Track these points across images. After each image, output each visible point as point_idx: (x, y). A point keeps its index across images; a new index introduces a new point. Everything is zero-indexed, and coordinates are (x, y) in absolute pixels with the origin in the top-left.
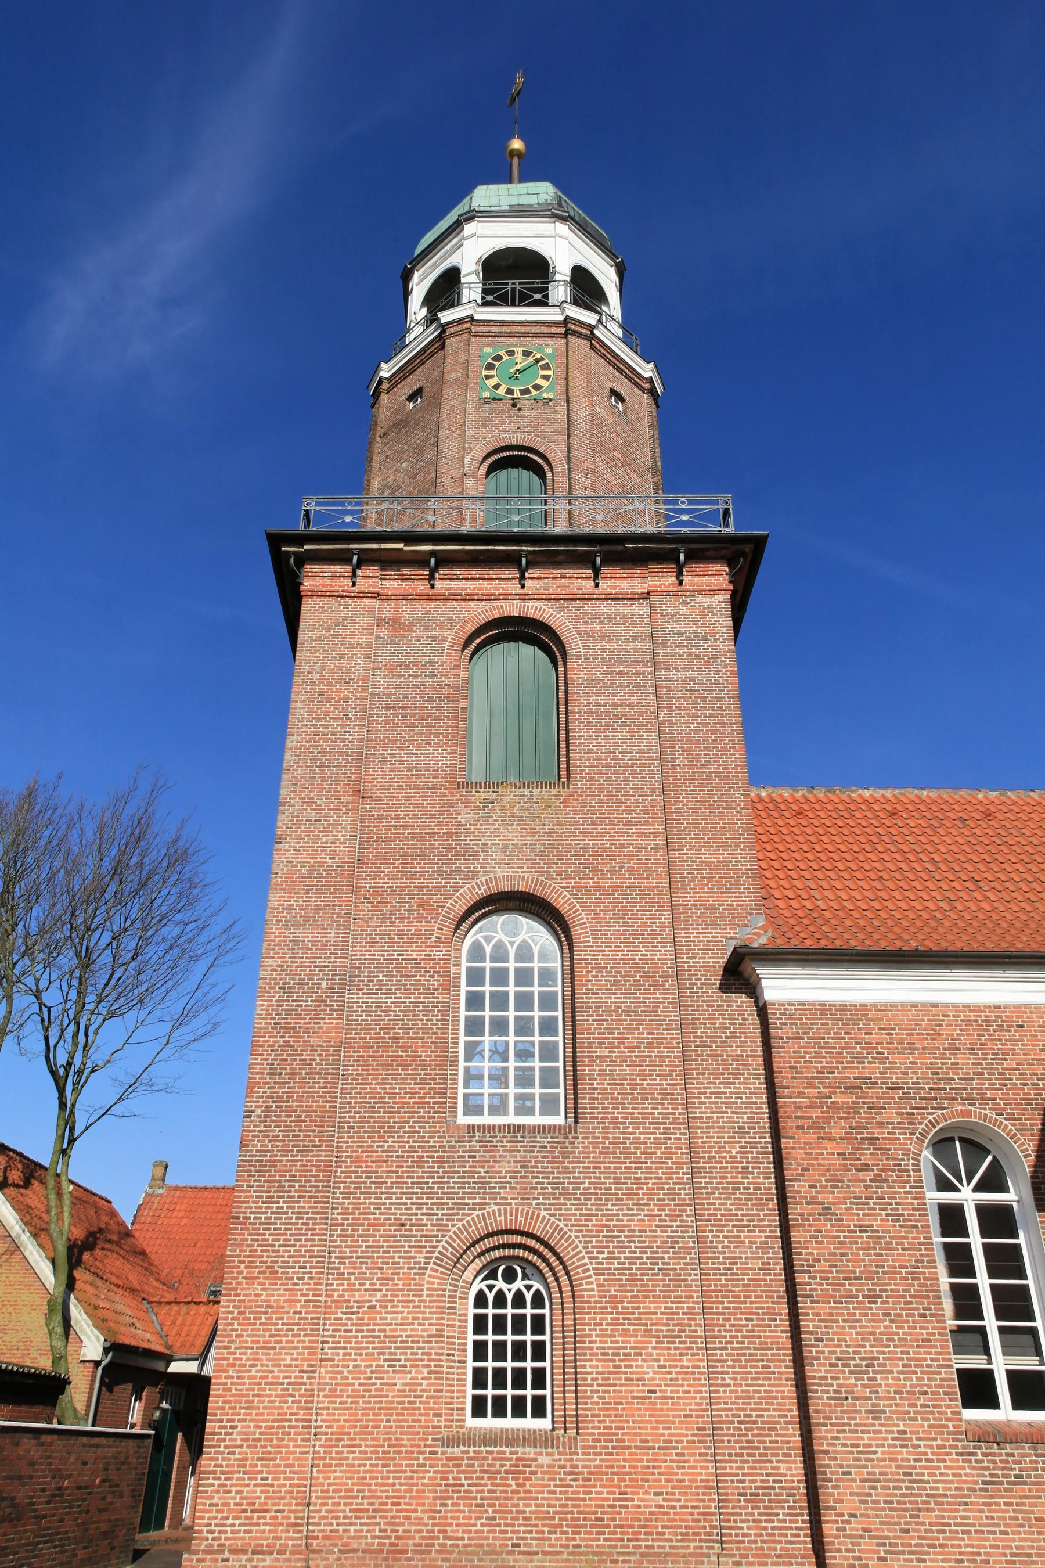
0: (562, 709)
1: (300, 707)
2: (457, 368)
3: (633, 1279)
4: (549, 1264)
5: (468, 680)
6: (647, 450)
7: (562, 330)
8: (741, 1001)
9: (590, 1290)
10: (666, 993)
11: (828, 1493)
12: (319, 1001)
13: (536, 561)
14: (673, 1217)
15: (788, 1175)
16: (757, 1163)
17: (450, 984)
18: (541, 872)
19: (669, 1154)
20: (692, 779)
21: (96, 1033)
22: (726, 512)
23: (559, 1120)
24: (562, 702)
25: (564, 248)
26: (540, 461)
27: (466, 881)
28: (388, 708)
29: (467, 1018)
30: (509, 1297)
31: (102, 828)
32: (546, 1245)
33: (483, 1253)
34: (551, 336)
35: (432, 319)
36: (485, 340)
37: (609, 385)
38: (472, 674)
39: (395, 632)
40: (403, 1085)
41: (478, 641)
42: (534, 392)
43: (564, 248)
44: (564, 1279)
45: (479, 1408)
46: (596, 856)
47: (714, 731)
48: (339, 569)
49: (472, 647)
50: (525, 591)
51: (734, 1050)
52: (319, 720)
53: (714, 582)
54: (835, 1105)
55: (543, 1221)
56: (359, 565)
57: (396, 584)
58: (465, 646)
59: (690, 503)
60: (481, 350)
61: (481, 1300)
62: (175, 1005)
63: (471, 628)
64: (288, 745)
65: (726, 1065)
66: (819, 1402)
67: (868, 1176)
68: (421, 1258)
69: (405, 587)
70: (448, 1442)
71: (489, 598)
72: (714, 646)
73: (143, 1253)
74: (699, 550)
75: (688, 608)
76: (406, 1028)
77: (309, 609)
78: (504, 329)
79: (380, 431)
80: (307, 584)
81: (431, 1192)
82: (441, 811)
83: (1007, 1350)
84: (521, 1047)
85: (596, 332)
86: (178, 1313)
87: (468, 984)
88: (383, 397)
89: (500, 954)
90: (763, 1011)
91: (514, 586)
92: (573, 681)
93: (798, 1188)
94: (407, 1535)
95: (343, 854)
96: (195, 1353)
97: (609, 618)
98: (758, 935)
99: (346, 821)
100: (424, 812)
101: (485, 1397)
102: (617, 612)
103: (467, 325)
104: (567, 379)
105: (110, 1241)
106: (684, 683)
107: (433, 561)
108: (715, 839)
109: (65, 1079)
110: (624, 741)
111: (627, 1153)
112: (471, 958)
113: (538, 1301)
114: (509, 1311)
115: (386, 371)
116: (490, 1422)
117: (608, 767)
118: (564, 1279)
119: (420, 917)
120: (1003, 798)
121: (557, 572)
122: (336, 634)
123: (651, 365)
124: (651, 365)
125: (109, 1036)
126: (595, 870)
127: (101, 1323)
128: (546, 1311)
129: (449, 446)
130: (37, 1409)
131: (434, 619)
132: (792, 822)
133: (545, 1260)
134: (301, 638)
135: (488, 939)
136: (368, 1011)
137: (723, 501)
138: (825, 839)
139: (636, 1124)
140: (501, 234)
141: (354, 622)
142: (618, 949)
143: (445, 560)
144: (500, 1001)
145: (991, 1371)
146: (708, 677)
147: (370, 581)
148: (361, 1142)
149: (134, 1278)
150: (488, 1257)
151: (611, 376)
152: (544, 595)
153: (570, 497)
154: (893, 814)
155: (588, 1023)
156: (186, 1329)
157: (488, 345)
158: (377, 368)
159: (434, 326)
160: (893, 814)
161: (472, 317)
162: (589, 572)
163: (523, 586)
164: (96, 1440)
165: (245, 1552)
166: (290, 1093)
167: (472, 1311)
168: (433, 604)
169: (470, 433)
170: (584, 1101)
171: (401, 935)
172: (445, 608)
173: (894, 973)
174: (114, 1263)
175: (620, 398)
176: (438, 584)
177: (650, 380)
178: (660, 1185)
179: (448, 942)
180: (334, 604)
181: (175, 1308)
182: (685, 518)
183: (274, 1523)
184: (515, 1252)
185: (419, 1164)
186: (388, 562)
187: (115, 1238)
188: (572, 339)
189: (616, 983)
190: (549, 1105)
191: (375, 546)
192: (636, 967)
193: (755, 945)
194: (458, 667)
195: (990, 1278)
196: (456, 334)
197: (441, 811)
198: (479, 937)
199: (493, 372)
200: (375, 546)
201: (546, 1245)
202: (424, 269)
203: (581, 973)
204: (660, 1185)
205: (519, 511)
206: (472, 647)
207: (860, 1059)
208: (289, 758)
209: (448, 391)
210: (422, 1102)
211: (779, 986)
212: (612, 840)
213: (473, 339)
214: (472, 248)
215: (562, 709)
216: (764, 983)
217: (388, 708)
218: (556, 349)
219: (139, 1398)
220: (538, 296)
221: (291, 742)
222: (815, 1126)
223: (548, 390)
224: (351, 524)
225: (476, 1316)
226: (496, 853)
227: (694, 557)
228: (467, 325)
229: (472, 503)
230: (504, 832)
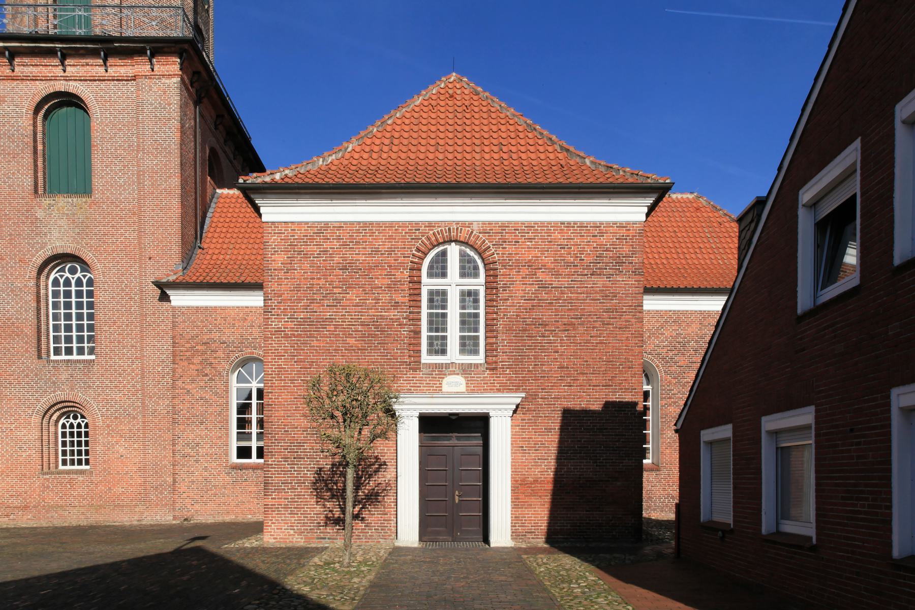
10: (135, 302)
14: (133, 395)
18: (78, 243)
19: (133, 371)
30: (75, 425)
40: (18, 343)
45: (64, 463)
46: (105, 235)
47: (166, 165)
50: (66, 74)
51: (163, 327)
55: (79, 396)
65: (158, 334)
67: (206, 378)
72: (169, 113)
75: (157, 86)
81: (32, 387)
82: (27, 211)
91: (58, 71)
106: (152, 136)
108: (162, 226)
111: (115, 371)
113: (87, 426)
116: (68, 467)
117: (112, 186)
119: (20, 267)
121: (84, 61)
126: (104, 242)
131: (17, 93)
135: (62, 276)
146: (165, 132)
162: (56, 62)
163: (65, 71)
168: (15, 83)
171: (12, 275)
172: (22, 85)
176: (17, 69)
184: (69, 409)
185: (27, 376)
192: (122, 290)
198: (57, 275)
207: (210, 331)
210: (27, 351)
212: (113, 226)
222: (188, 359)
230: (59, 222)
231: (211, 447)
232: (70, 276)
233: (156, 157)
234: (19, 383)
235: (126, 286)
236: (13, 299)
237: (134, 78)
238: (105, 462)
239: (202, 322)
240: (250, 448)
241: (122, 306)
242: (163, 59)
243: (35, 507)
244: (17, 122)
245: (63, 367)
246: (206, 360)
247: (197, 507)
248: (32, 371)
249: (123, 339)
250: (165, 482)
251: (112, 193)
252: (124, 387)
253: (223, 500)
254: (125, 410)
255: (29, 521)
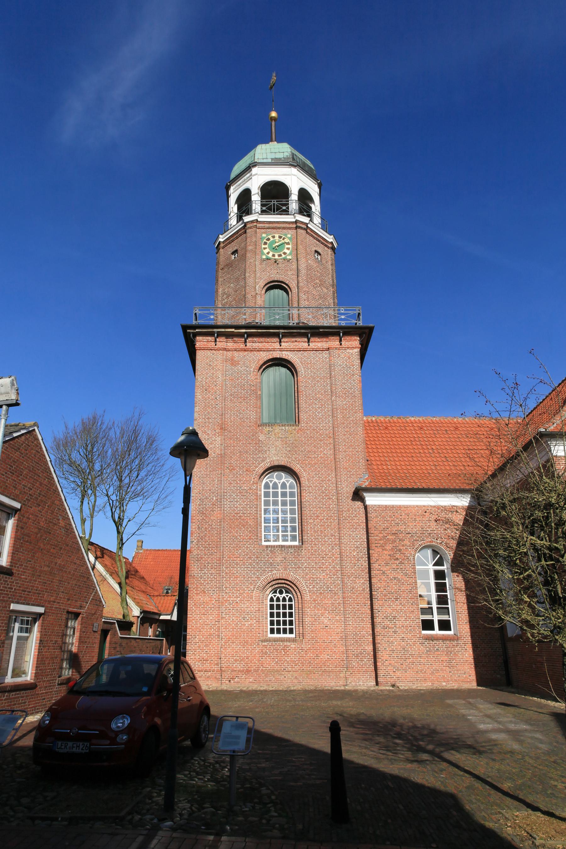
0: (296, 395)
1: (199, 395)
2: (252, 244)
3: (321, 593)
4: (294, 589)
5: (261, 383)
6: (330, 276)
7: (294, 226)
8: (359, 504)
9: (307, 597)
11: (379, 654)
12: (213, 504)
13: (285, 335)
14: (334, 575)
15: (371, 562)
16: (362, 557)
17: (258, 498)
20: (344, 423)
21: (126, 506)
22: (359, 314)
23: (296, 543)
24: (296, 392)
25: (295, 180)
26: (286, 287)
27: (263, 461)
28: (231, 395)
29: (264, 500)
30: (281, 599)
31: (122, 429)
32: (293, 583)
33: (272, 586)
34: (290, 228)
35: (240, 218)
36: (263, 230)
37: (314, 249)
38: (262, 380)
39: (232, 364)
40: (243, 532)
41: (264, 367)
42: (283, 256)
43: (295, 180)
44: (299, 594)
45: (272, 631)
47: (352, 405)
48: (210, 338)
49: (262, 369)
51: (356, 520)
52: (206, 400)
53: (354, 342)
54: (388, 539)
56: (217, 337)
57: (232, 344)
58: (259, 370)
59: (345, 310)
60: (261, 235)
61: (272, 600)
62: (155, 497)
63: (261, 362)
64: (196, 410)
65: (353, 526)
66: (378, 629)
68: (252, 587)
69: (235, 346)
70: (263, 641)
71: (268, 350)
73: (143, 578)
74: (348, 331)
75: (343, 354)
76: (244, 513)
77: (199, 355)
78: (271, 225)
79: (221, 267)
80: (198, 345)
81: (254, 567)
82: (253, 435)
83: (439, 614)
84: (283, 519)
85: (309, 225)
86: (161, 599)
87: (264, 497)
88: (221, 250)
89: (275, 486)
90: (366, 507)
91: (277, 345)
92: (300, 384)
93: (375, 566)
94: (251, 667)
95: (218, 451)
96: (169, 613)
97: (314, 359)
98: (365, 482)
99: (218, 439)
100: (247, 436)
101: (273, 605)
102: (317, 356)
103: (255, 224)
104: (297, 249)
105: (132, 575)
106: (342, 386)
107: (246, 335)
108: (351, 446)
109: (118, 524)
110: (319, 408)
111: (319, 554)
112: (265, 488)
113: (290, 600)
114: (281, 603)
115: (222, 238)
116: (276, 635)
117: (313, 418)
118: (299, 594)
119: (247, 474)
120: (464, 421)
121: (294, 339)
122: (210, 365)
123: (332, 236)
124: (332, 236)
125: (131, 508)
126: (308, 457)
127: (138, 604)
128: (293, 603)
129: (250, 281)
130: (126, 632)
131: (247, 359)
132: (383, 432)
133: (292, 588)
134: (198, 367)
136: (230, 508)
137: (358, 309)
138: (394, 439)
139: (322, 545)
140: (268, 174)
141: (216, 361)
142: (316, 486)
143: (250, 335)
144: (275, 495)
145: (433, 620)
147: (222, 343)
148: (230, 551)
149: (143, 587)
150: (274, 587)
151: (315, 245)
152: (287, 349)
153: (299, 308)
154: (421, 428)
155: (306, 512)
156: (164, 605)
157: (264, 233)
158: (218, 237)
159: (241, 222)
160: (421, 428)
161: (257, 220)
162: (306, 340)
163: (281, 346)
164: (149, 641)
165: (202, 671)
166: (205, 535)
167: (269, 603)
168: (246, 353)
169: (258, 275)
170: (305, 538)
171: (240, 480)
172: (251, 354)
173: (411, 495)
174: (136, 582)
175: (319, 254)
176: (248, 344)
177: (332, 243)
178: (330, 565)
179: (257, 483)
180: (209, 353)
181: (160, 597)
182: (343, 317)
183: (210, 663)
184: (283, 586)
185: (250, 558)
186: (228, 336)
187: (133, 573)
188: (300, 231)
189: (316, 498)
190: (294, 538)
191: (223, 330)
192: (323, 492)
193: (363, 486)
194: (257, 379)
195: (437, 592)
196: (251, 228)
197: (253, 435)
198: (267, 480)
199: (266, 246)
200: (223, 330)
201: (293, 583)
202: (235, 186)
203: (303, 494)
204: (330, 565)
205: (279, 314)
206: (262, 369)
207: (398, 524)
208: (196, 415)
209: (248, 255)
210: (250, 538)
211: (372, 500)
212: (315, 446)
213: (258, 230)
214: (256, 180)
215: (296, 395)
216: (366, 499)
217: (231, 395)
218: (292, 235)
219: (151, 628)
220: (284, 208)
221: (197, 409)
222: (381, 546)
223: (289, 255)
224: (213, 319)
225: (270, 605)
226: (273, 451)
227: (345, 334)
228: (255, 224)
229: (261, 308)
231: (406, 620)
232: (277, 481)
233: (345, 399)
234: (244, 564)
235: (326, 489)
236: (240, 498)
237: (328, 349)
238: (312, 631)
239: (390, 517)
240: (432, 621)
241: (323, 504)
242: (348, 338)
243: (256, 671)
244: (247, 377)
245: (278, 552)
246: (396, 546)
247: (398, 674)
248: (254, 554)
249: (325, 529)
250: (364, 650)
251: (313, 423)
252: (327, 567)
253: (419, 668)
254: (328, 587)
255: (251, 684)
